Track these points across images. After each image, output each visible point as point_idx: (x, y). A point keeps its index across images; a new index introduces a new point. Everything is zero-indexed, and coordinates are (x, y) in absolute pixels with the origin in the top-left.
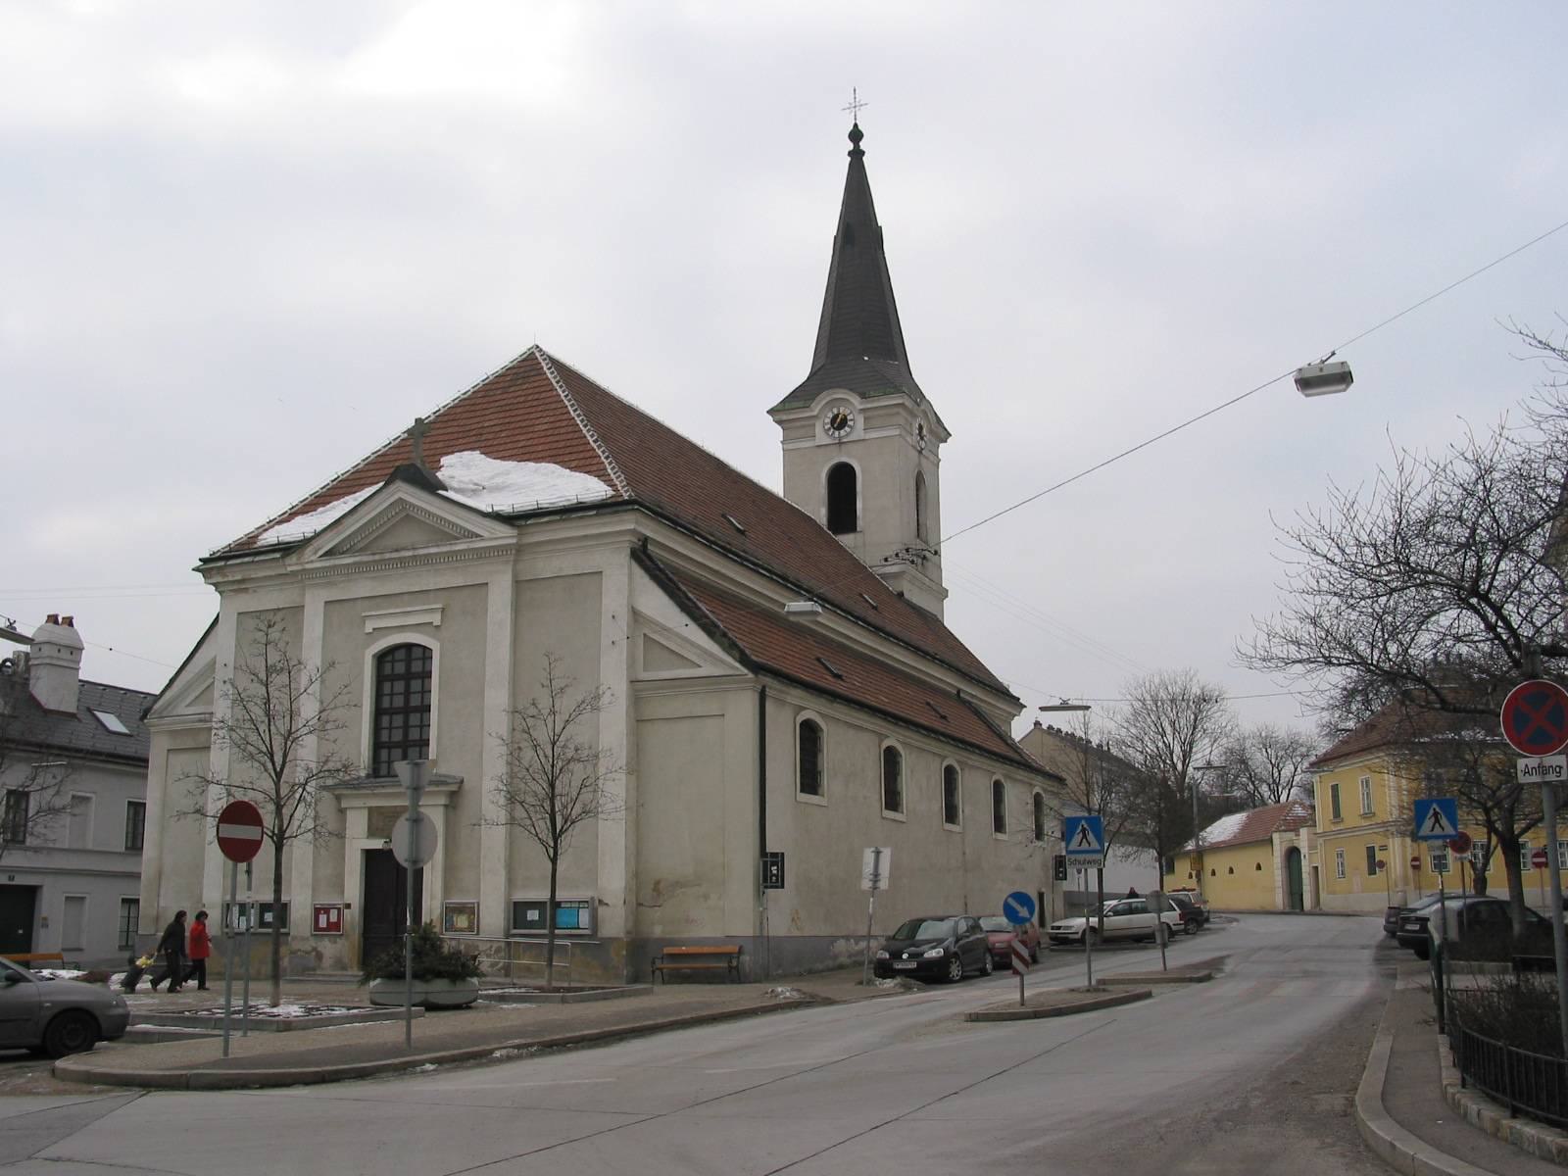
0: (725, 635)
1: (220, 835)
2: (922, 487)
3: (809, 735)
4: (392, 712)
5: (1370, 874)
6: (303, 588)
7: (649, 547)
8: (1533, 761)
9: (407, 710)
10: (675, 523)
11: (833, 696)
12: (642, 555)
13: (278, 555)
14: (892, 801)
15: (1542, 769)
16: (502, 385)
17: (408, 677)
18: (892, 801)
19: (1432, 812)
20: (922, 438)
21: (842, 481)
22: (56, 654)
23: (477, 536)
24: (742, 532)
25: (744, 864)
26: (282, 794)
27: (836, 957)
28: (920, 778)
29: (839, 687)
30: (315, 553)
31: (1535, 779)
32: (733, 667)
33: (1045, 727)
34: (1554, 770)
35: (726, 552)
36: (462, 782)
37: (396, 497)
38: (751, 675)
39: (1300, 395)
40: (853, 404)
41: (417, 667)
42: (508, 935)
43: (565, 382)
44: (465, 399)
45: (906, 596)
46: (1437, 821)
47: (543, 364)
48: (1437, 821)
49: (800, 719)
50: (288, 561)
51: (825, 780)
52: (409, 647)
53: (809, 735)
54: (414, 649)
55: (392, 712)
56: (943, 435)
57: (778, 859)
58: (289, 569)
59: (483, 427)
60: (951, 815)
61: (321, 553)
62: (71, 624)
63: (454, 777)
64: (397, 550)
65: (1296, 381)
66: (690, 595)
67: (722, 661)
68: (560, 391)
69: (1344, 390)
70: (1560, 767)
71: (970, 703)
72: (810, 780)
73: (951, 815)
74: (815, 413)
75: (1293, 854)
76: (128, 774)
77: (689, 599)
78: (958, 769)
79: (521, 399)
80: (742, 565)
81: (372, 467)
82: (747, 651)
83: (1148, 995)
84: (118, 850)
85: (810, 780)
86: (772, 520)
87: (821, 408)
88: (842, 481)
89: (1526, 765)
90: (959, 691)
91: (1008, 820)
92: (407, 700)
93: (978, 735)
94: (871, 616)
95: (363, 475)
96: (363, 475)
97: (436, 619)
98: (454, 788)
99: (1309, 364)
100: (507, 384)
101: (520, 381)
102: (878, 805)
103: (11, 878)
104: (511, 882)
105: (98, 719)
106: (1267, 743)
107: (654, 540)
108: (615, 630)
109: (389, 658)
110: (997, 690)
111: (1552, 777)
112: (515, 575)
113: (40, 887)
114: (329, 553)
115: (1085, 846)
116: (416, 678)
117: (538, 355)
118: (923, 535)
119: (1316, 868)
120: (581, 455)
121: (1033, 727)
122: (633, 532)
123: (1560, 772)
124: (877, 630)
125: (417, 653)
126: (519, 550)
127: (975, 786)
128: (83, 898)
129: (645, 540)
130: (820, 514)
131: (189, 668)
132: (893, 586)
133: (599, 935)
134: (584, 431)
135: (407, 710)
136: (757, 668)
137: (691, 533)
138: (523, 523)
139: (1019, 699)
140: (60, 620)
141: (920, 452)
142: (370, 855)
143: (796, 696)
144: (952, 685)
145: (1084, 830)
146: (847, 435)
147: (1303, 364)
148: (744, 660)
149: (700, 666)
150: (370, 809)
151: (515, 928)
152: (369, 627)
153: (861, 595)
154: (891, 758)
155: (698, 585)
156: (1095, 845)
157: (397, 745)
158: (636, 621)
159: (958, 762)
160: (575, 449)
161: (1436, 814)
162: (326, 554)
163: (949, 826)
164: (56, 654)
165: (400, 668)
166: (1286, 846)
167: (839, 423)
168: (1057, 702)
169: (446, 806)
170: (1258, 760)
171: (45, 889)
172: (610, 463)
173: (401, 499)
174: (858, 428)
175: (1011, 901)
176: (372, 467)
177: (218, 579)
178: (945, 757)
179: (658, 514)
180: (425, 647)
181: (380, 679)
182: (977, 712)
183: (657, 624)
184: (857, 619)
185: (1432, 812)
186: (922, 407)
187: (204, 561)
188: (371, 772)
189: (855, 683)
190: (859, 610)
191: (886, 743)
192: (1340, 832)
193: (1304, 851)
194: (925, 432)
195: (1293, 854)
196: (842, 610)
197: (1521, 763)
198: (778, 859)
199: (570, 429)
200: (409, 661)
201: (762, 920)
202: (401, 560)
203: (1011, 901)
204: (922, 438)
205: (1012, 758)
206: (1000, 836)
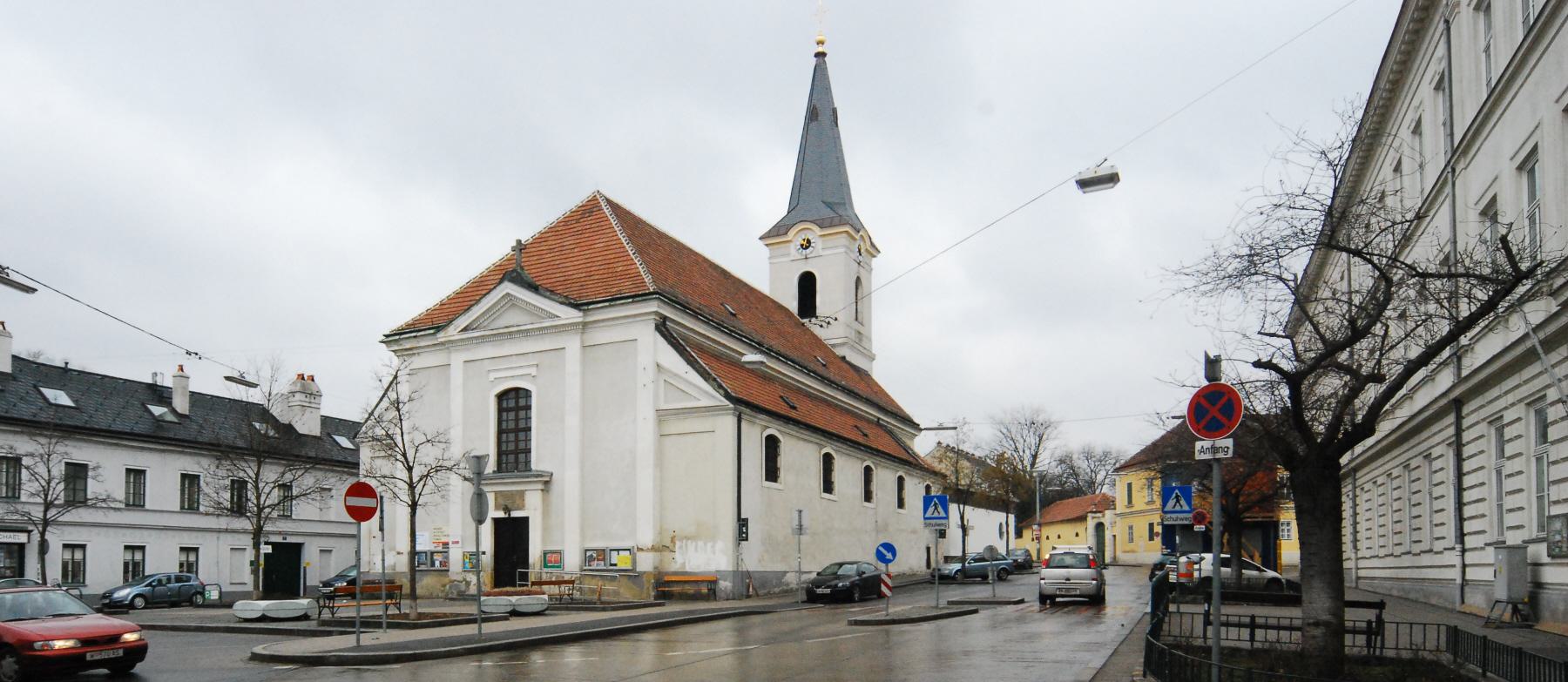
0: (715, 380)
1: (348, 504)
2: (860, 287)
3: (772, 445)
4: (507, 431)
5: (1150, 540)
6: (450, 352)
7: (667, 323)
8: (1207, 443)
9: (517, 430)
10: (684, 308)
11: (787, 420)
12: (663, 327)
13: (432, 331)
14: (828, 487)
15: (1214, 449)
16: (575, 218)
17: (517, 409)
18: (828, 487)
19: (1174, 495)
20: (860, 255)
21: (807, 284)
22: (304, 399)
23: (557, 317)
24: (734, 315)
25: (729, 526)
26: (414, 481)
27: (788, 584)
28: (848, 470)
29: (793, 414)
30: (455, 330)
31: (1208, 456)
32: (721, 401)
33: (944, 445)
34: (1223, 450)
35: (719, 327)
36: (552, 474)
37: (504, 293)
38: (731, 406)
39: (1080, 192)
40: (815, 233)
41: (522, 402)
42: (582, 570)
43: (616, 215)
44: (551, 228)
45: (848, 359)
46: (1178, 501)
47: (602, 203)
48: (936, 508)
49: (765, 435)
50: (439, 335)
51: (782, 474)
52: (517, 390)
53: (772, 445)
54: (521, 392)
55: (507, 431)
56: (874, 250)
57: (746, 520)
58: (440, 340)
59: (563, 246)
60: (868, 496)
61: (460, 329)
62: (313, 380)
63: (548, 472)
64: (507, 327)
65: (1077, 182)
66: (693, 353)
67: (713, 397)
68: (612, 221)
69: (1112, 187)
70: (1228, 448)
71: (885, 426)
72: (772, 473)
73: (868, 496)
74: (789, 239)
75: (1100, 527)
76: (143, 449)
77: (693, 357)
78: (873, 467)
79: (588, 227)
80: (730, 335)
81: (492, 273)
82: (729, 390)
83: (976, 611)
84: (176, 510)
85: (772, 473)
86: (757, 308)
87: (795, 236)
88: (807, 284)
89: (1202, 447)
90: (879, 419)
91: (907, 500)
92: (517, 425)
93: (885, 444)
94: (821, 370)
95: (486, 278)
96: (486, 278)
97: (533, 371)
98: (547, 479)
99: (1088, 169)
100: (579, 217)
101: (587, 215)
102: (818, 490)
103: (285, 539)
104: (583, 536)
105: (334, 440)
106: (1088, 456)
107: (671, 319)
108: (646, 376)
109: (504, 398)
110: (903, 418)
111: (1220, 455)
112: (582, 342)
113: (303, 544)
114: (465, 329)
115: (936, 515)
116: (522, 410)
117: (598, 196)
118: (859, 318)
119: (1114, 536)
120: (625, 263)
121: (936, 445)
122: (656, 313)
123: (1227, 452)
124: (823, 379)
125: (522, 394)
126: (585, 325)
127: (885, 478)
128: (331, 551)
129: (665, 318)
130: (793, 305)
131: (1369, 570)
132: (840, 352)
133: (638, 570)
134: (627, 247)
135: (517, 430)
136: (736, 401)
137: (696, 314)
138: (586, 308)
139: (918, 425)
140: (306, 378)
141: (859, 264)
142: (496, 521)
143: (762, 419)
144: (875, 416)
145: (935, 504)
146: (811, 253)
147: (1083, 169)
148: (727, 396)
149: (699, 400)
150: (496, 493)
151: (22, 546)
152: (492, 376)
153: (815, 357)
154: (828, 460)
155: (701, 349)
156: (943, 514)
157: (512, 452)
158: (659, 371)
159: (873, 463)
160: (620, 259)
161: (1177, 497)
162: (462, 331)
163: (867, 504)
164: (304, 399)
165: (512, 404)
166: (1096, 521)
167: (807, 245)
168: (936, 425)
169: (542, 490)
170: (1082, 465)
171: (306, 545)
172: (643, 268)
173: (508, 294)
174: (818, 244)
175: (881, 549)
176: (492, 273)
177: (396, 348)
178: (865, 460)
179: (673, 302)
180: (527, 390)
181: (500, 410)
182: (890, 433)
183: (670, 372)
184: (810, 372)
185: (1174, 495)
186: (861, 233)
187: (387, 336)
188: (496, 469)
189: (805, 411)
190: (812, 366)
191: (825, 451)
192: (1132, 513)
193: (1107, 525)
194: (862, 251)
195: (1100, 527)
196: (783, 357)
197: (1198, 445)
198: (746, 520)
199: (619, 246)
200: (517, 399)
201: (738, 559)
202: (510, 333)
203: (881, 549)
204: (860, 255)
205: (911, 462)
206: (900, 511)
